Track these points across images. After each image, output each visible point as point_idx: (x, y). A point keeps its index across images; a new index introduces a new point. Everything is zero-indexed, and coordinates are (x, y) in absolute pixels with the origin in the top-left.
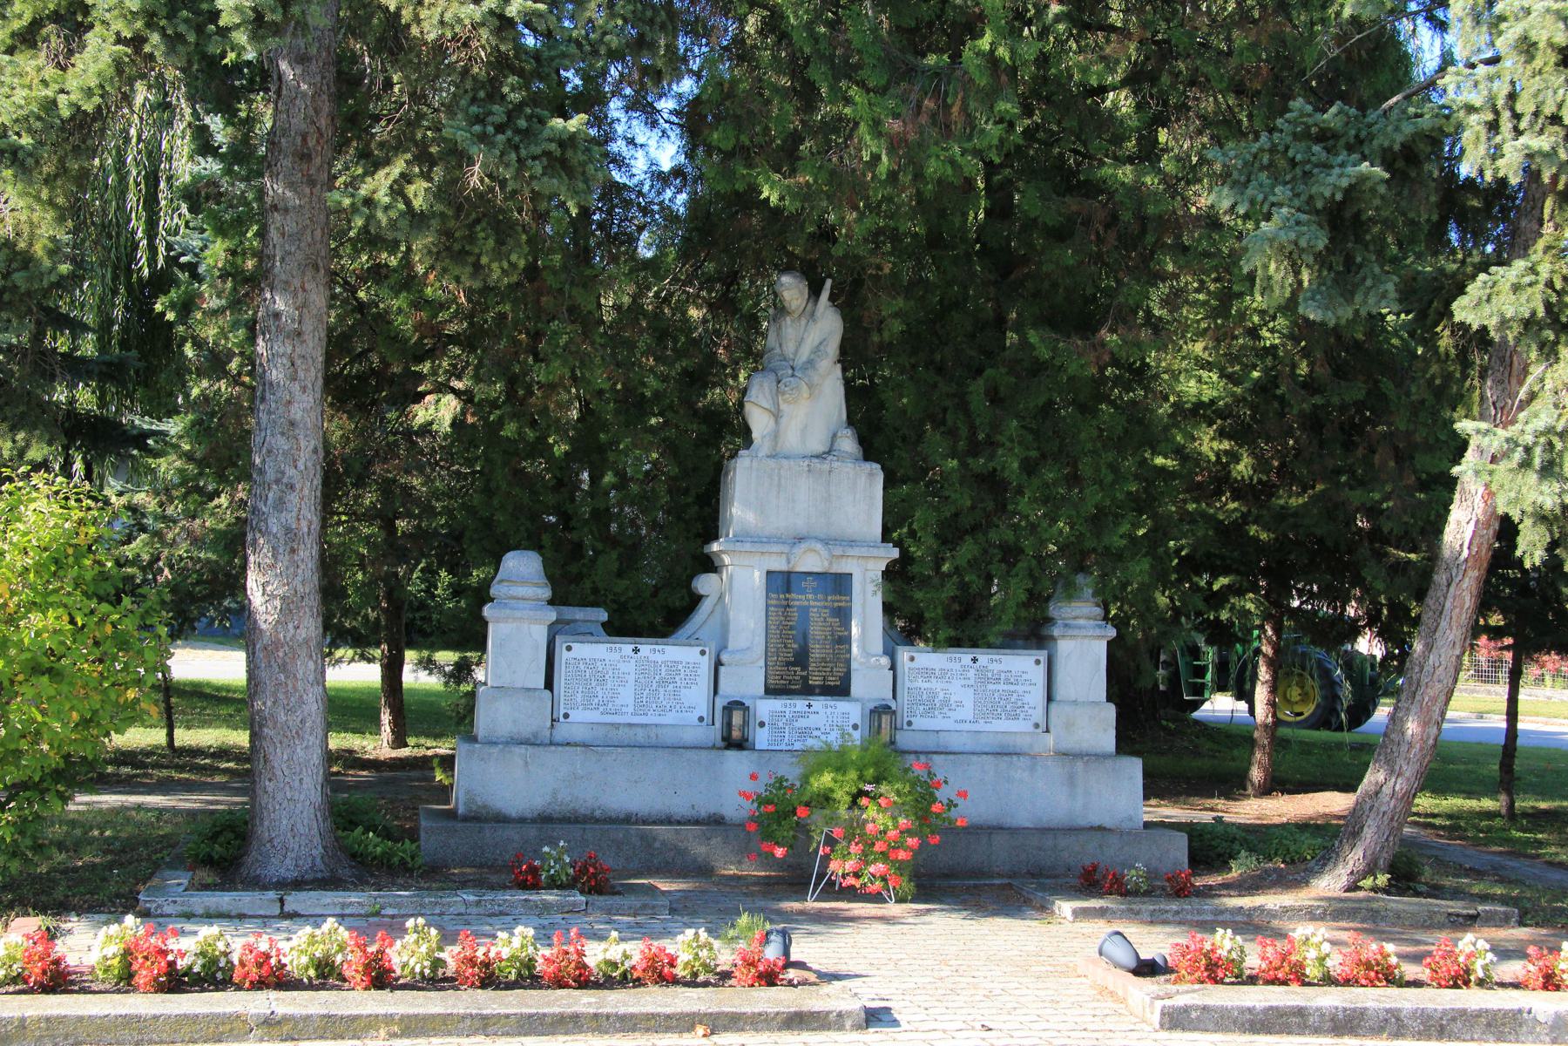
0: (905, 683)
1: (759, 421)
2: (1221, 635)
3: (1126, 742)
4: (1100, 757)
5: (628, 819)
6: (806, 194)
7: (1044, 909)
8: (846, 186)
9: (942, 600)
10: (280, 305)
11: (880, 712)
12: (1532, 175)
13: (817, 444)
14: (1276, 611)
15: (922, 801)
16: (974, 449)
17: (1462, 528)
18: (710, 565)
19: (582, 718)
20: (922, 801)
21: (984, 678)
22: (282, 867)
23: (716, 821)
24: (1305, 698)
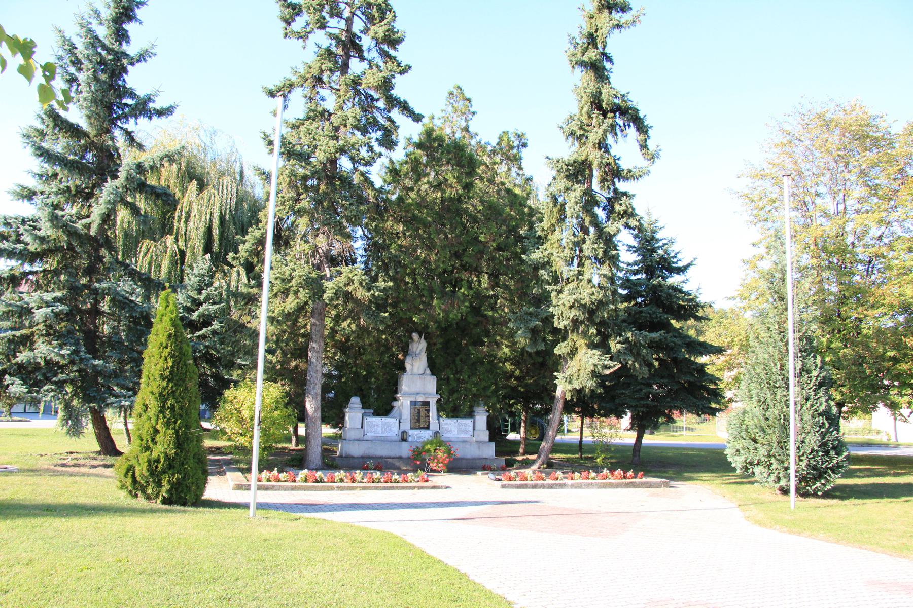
0: (442, 426)
1: (408, 366)
2: (512, 415)
3: (491, 439)
4: (484, 442)
5: (381, 457)
6: (423, 319)
7: (475, 473)
8: (432, 318)
9: (454, 406)
10: (315, 345)
11: (437, 433)
12: (565, 327)
13: (421, 372)
14: (527, 409)
15: (449, 452)
16: (457, 373)
17: (558, 393)
18: (396, 400)
19: (370, 435)
20: (449, 452)
21: (460, 425)
22: (314, 466)
23: (400, 458)
24: (536, 433)
